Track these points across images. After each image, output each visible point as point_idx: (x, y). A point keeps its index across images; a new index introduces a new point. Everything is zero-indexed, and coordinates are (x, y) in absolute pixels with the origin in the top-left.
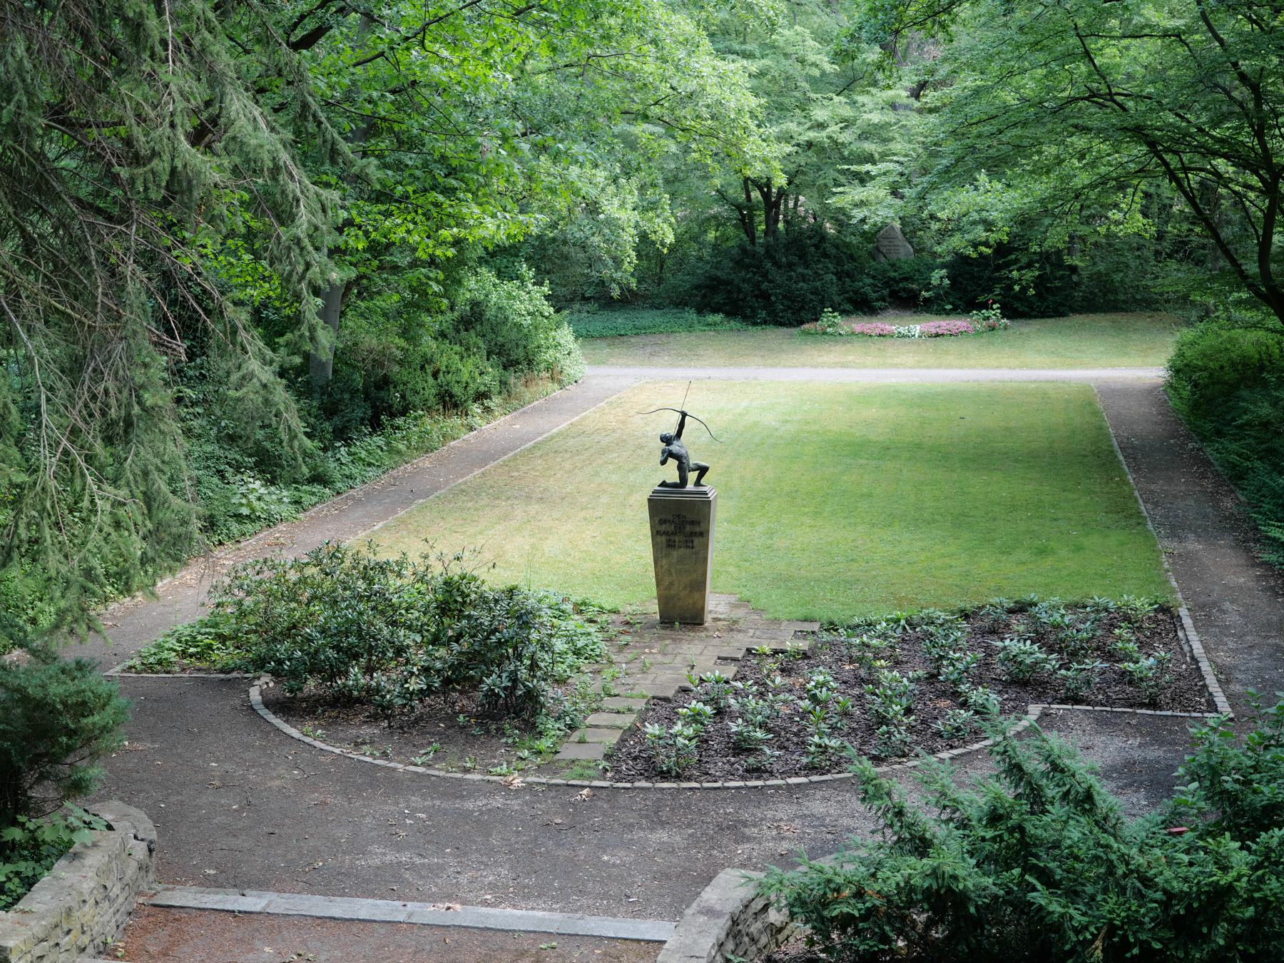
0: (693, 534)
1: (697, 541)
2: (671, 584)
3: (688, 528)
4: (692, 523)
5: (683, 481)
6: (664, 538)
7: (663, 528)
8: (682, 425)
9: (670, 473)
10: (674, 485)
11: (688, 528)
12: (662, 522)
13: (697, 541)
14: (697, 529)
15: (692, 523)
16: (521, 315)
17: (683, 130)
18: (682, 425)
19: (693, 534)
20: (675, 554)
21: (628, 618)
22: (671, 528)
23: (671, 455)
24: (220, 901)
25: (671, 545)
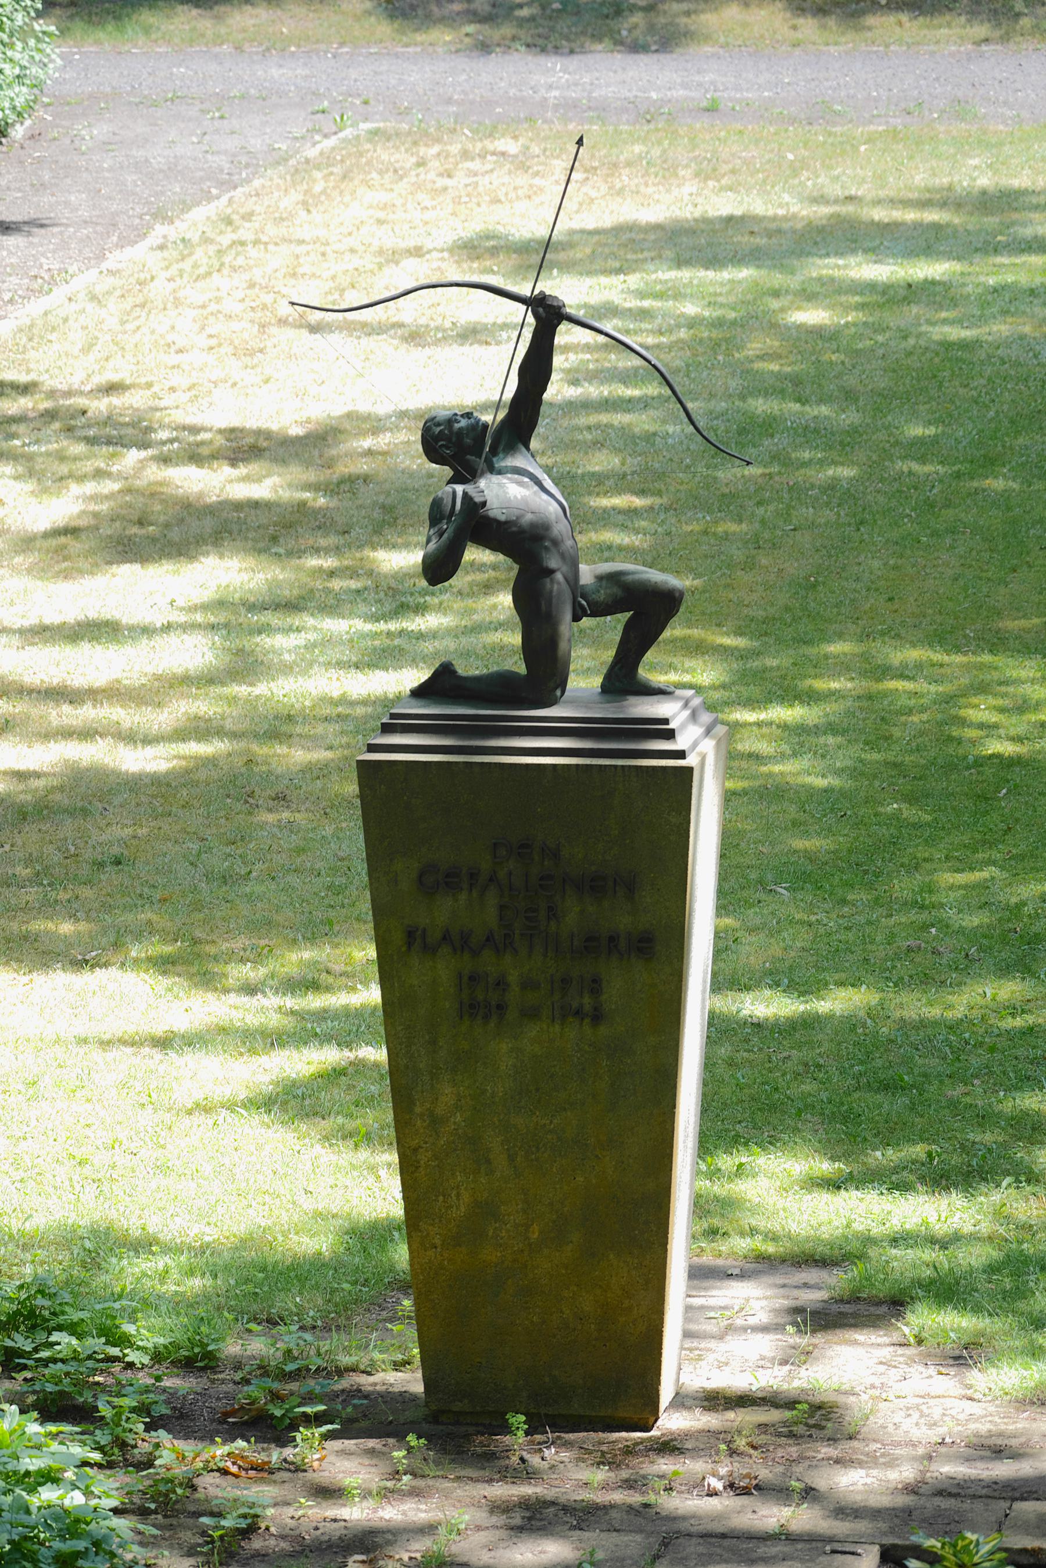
0: (597, 944)
1: (619, 981)
2: (486, 1211)
3: (574, 914)
4: (595, 885)
5: (543, 672)
6: (444, 970)
7: (444, 912)
8: (536, 368)
9: (479, 619)
10: (499, 690)
11: (574, 914)
12: (437, 881)
13: (619, 981)
14: (622, 921)
15: (595, 885)
16: (54, 1436)
17: (303, 241)
18: (536, 368)
19: (597, 944)
20: (507, 1051)
21: (256, 1391)
22: (484, 914)
23: (477, 525)
24: (686, 1147)
25: (481, 1003)
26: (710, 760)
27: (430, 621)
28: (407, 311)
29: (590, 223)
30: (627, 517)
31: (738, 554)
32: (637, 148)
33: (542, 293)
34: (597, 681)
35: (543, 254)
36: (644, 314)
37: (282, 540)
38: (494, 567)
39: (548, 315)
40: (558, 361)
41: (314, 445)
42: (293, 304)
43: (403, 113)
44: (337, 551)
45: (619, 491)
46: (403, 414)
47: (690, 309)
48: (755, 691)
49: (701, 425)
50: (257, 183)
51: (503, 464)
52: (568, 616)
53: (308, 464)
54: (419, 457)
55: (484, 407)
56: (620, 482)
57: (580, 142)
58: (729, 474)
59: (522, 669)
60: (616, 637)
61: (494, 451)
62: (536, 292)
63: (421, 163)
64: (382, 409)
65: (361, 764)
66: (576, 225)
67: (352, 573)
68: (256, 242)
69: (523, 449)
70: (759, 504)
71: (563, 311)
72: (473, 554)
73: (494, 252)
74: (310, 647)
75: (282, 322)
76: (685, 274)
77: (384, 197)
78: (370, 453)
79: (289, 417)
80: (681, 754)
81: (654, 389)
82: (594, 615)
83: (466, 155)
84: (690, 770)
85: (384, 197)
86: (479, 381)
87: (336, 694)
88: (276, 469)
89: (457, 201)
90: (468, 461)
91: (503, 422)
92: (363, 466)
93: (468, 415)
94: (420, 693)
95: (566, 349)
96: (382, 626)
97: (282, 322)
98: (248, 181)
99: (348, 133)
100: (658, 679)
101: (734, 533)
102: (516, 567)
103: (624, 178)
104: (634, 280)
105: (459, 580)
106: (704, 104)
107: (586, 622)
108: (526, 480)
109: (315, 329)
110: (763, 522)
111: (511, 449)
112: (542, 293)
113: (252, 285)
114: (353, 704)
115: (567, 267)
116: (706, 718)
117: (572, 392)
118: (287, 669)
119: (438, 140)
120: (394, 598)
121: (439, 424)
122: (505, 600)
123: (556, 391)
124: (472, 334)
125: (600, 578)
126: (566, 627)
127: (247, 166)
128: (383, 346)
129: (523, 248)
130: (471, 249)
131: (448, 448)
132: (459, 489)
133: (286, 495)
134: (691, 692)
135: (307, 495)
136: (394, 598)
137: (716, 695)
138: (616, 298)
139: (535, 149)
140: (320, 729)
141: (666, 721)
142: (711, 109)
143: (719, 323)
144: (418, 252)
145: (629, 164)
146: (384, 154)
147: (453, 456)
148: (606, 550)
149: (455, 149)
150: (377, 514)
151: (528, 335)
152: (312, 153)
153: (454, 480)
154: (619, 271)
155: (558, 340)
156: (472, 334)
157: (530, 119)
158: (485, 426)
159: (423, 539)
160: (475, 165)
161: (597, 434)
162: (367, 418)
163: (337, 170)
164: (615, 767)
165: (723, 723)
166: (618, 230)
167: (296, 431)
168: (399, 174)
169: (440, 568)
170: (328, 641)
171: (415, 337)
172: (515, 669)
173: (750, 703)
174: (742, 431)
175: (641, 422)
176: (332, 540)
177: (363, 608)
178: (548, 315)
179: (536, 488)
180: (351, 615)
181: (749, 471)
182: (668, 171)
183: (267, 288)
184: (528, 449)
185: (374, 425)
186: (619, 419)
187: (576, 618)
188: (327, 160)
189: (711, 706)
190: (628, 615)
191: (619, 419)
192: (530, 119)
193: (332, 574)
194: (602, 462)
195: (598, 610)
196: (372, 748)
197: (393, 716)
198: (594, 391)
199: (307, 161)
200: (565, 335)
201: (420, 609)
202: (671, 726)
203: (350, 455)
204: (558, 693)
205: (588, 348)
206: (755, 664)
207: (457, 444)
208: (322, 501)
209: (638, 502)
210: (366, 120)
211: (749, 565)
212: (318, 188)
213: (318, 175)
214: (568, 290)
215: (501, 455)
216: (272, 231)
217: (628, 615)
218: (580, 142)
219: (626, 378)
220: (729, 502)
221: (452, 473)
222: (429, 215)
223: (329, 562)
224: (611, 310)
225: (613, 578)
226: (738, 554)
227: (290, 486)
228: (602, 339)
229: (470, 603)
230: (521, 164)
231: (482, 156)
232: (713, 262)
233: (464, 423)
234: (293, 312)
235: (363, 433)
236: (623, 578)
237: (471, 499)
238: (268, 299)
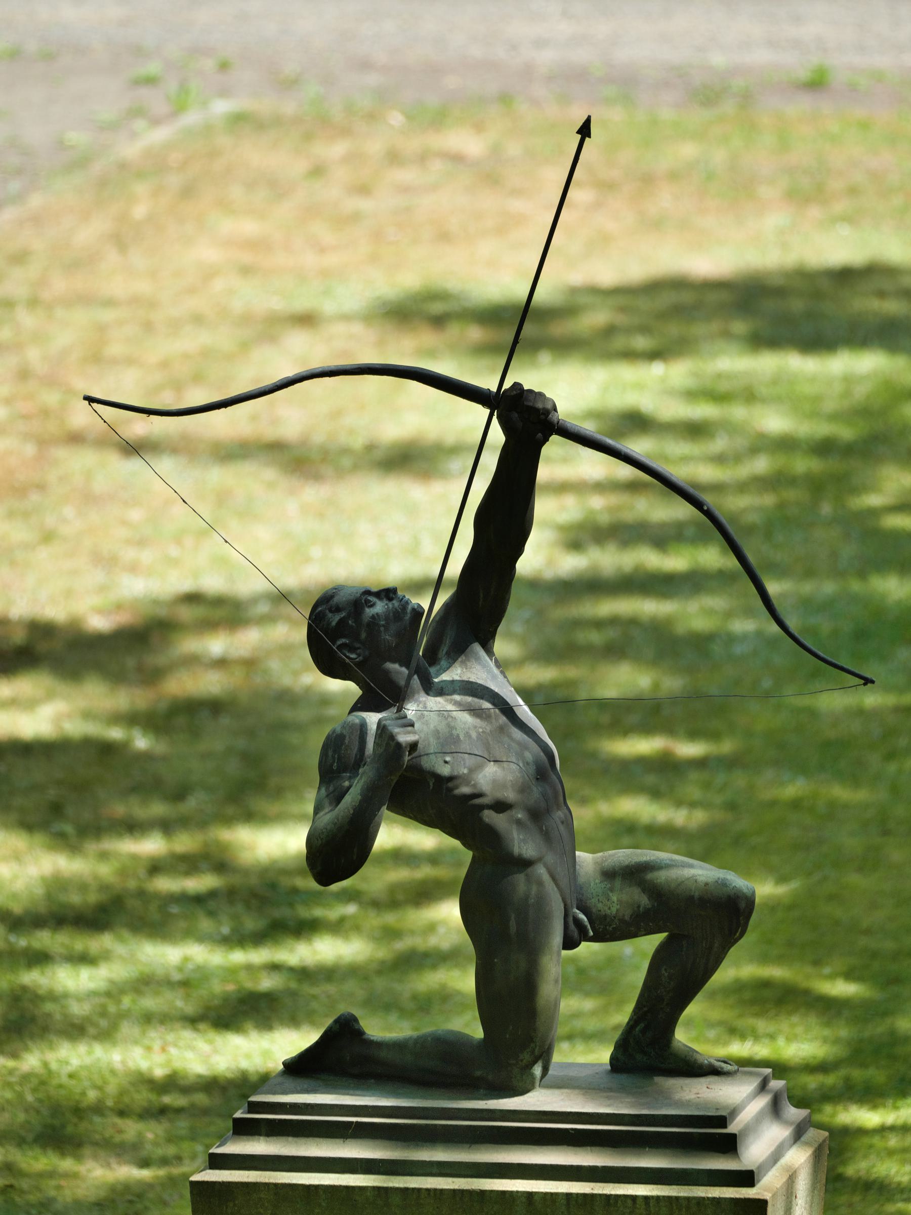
8: (504, 516)
9: (405, 938)
10: (437, 1066)
18: (504, 516)
26: (802, 1185)
27: (324, 950)
28: (289, 417)
29: (607, 272)
30: (661, 775)
31: (851, 842)
32: (688, 150)
33: (517, 386)
34: (603, 1055)
35: (520, 326)
36: (695, 430)
37: (70, 811)
38: (433, 858)
39: (527, 423)
40: (544, 508)
41: (132, 647)
42: (90, 400)
43: (288, 85)
44: (166, 827)
45: (646, 729)
46: (283, 597)
47: (774, 422)
48: (877, 1075)
49: (793, 623)
50: (36, 201)
51: (446, 677)
52: (557, 938)
53: (116, 677)
54: (307, 669)
55: (418, 586)
56: (646, 714)
57: (585, 130)
58: (834, 701)
59: (473, 1029)
60: (638, 978)
61: (432, 656)
62: (507, 385)
63: (318, 171)
64: (249, 586)
65: (199, 1188)
66: (577, 277)
67: (188, 864)
68: (33, 303)
69: (482, 653)
70: (891, 756)
71: (553, 417)
72: (392, 834)
73: (439, 321)
74: (114, 992)
75: (76, 439)
76: (767, 364)
77: (249, 227)
78: (221, 663)
79: (89, 600)
80: (747, 1178)
81: (713, 557)
82: (598, 938)
83: (394, 158)
84: (761, 1205)
85: (249, 227)
86: (411, 541)
87: (159, 1073)
88: (61, 687)
89: (377, 236)
90: (387, 673)
91: (447, 606)
92: (210, 684)
93: (388, 593)
94: (301, 1068)
95: (562, 488)
96: (239, 957)
97: (76, 439)
98: (19, 198)
99: (192, 118)
100: (710, 1049)
101: (846, 806)
102: (468, 855)
103: (665, 200)
104: (677, 372)
105: (371, 879)
106: (804, 74)
107: (586, 948)
108: (487, 705)
109: (133, 448)
110: (895, 789)
111: (459, 651)
112: (517, 386)
113: (24, 374)
114: (186, 1090)
115: (566, 347)
116: (794, 1113)
117: (571, 564)
118: (76, 1030)
119: (345, 132)
120: (265, 907)
121: (337, 609)
122: (449, 912)
123: (537, 557)
124: (407, 459)
125: (610, 874)
126: (557, 963)
127: (19, 172)
128: (253, 480)
129: (490, 315)
130: (403, 313)
131: (352, 649)
132: (372, 719)
133: (75, 728)
134: (769, 1070)
135: (116, 734)
136: (265, 907)
137: (812, 1082)
138: (646, 403)
139: (514, 149)
140: (131, 1129)
141: (722, 1121)
142: (816, 84)
143: (824, 448)
144: (306, 320)
145: (674, 176)
146: (257, 155)
147: (359, 665)
148: (627, 830)
149: (375, 146)
150: (234, 768)
151: (490, 462)
152: (130, 150)
153: (365, 704)
154: (654, 355)
155: (544, 472)
156: (407, 459)
157: (505, 99)
158: (418, 613)
159: (310, 808)
160: (407, 175)
161: (611, 634)
162: (219, 601)
163: (174, 181)
164: (634, 1198)
165: (820, 1126)
166: (654, 287)
167: (99, 623)
168: (278, 189)
169: (338, 854)
170: (145, 983)
171: (298, 460)
172: (467, 1031)
173: (870, 1095)
174: (861, 635)
175: (694, 614)
176: (158, 809)
177: (205, 924)
178: (527, 423)
179: (503, 719)
180: (191, 934)
181: (871, 699)
182: (737, 190)
183: (51, 381)
184: (489, 652)
185: (225, 612)
186: (648, 607)
187: (569, 943)
188: (154, 165)
189: (794, 1092)
190: (658, 938)
191: (648, 607)
192: (505, 99)
193: (156, 867)
194: (625, 679)
195: (608, 930)
196: (218, 1162)
197: (254, 1107)
198: (609, 560)
199: (123, 166)
200: (557, 462)
201: (305, 929)
202: (732, 1128)
203: (193, 661)
204: (537, 1070)
205: (600, 487)
206: (878, 1029)
207: (355, 632)
208: (141, 742)
209: (689, 749)
210: (224, 92)
211: (870, 861)
212: (140, 211)
213: (141, 189)
214: (570, 388)
215: (444, 663)
216: (59, 285)
217: (658, 938)
218: (585, 130)
219: (661, 537)
220: (835, 753)
221: (360, 692)
222: (332, 260)
223: (152, 846)
224: (637, 422)
225: (635, 874)
226: (851, 842)
227: (87, 715)
228: (626, 471)
229: (390, 918)
230: (489, 174)
231: (423, 158)
232: (817, 341)
233: (380, 607)
234: (82, 417)
235: (209, 626)
236: (650, 876)
237: (392, 737)
238: (51, 398)
